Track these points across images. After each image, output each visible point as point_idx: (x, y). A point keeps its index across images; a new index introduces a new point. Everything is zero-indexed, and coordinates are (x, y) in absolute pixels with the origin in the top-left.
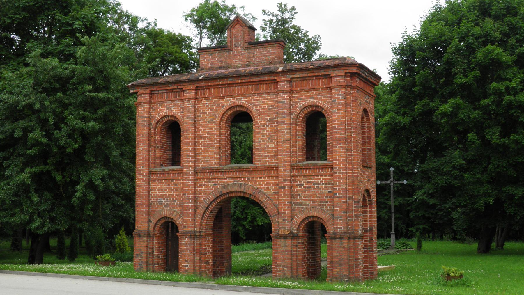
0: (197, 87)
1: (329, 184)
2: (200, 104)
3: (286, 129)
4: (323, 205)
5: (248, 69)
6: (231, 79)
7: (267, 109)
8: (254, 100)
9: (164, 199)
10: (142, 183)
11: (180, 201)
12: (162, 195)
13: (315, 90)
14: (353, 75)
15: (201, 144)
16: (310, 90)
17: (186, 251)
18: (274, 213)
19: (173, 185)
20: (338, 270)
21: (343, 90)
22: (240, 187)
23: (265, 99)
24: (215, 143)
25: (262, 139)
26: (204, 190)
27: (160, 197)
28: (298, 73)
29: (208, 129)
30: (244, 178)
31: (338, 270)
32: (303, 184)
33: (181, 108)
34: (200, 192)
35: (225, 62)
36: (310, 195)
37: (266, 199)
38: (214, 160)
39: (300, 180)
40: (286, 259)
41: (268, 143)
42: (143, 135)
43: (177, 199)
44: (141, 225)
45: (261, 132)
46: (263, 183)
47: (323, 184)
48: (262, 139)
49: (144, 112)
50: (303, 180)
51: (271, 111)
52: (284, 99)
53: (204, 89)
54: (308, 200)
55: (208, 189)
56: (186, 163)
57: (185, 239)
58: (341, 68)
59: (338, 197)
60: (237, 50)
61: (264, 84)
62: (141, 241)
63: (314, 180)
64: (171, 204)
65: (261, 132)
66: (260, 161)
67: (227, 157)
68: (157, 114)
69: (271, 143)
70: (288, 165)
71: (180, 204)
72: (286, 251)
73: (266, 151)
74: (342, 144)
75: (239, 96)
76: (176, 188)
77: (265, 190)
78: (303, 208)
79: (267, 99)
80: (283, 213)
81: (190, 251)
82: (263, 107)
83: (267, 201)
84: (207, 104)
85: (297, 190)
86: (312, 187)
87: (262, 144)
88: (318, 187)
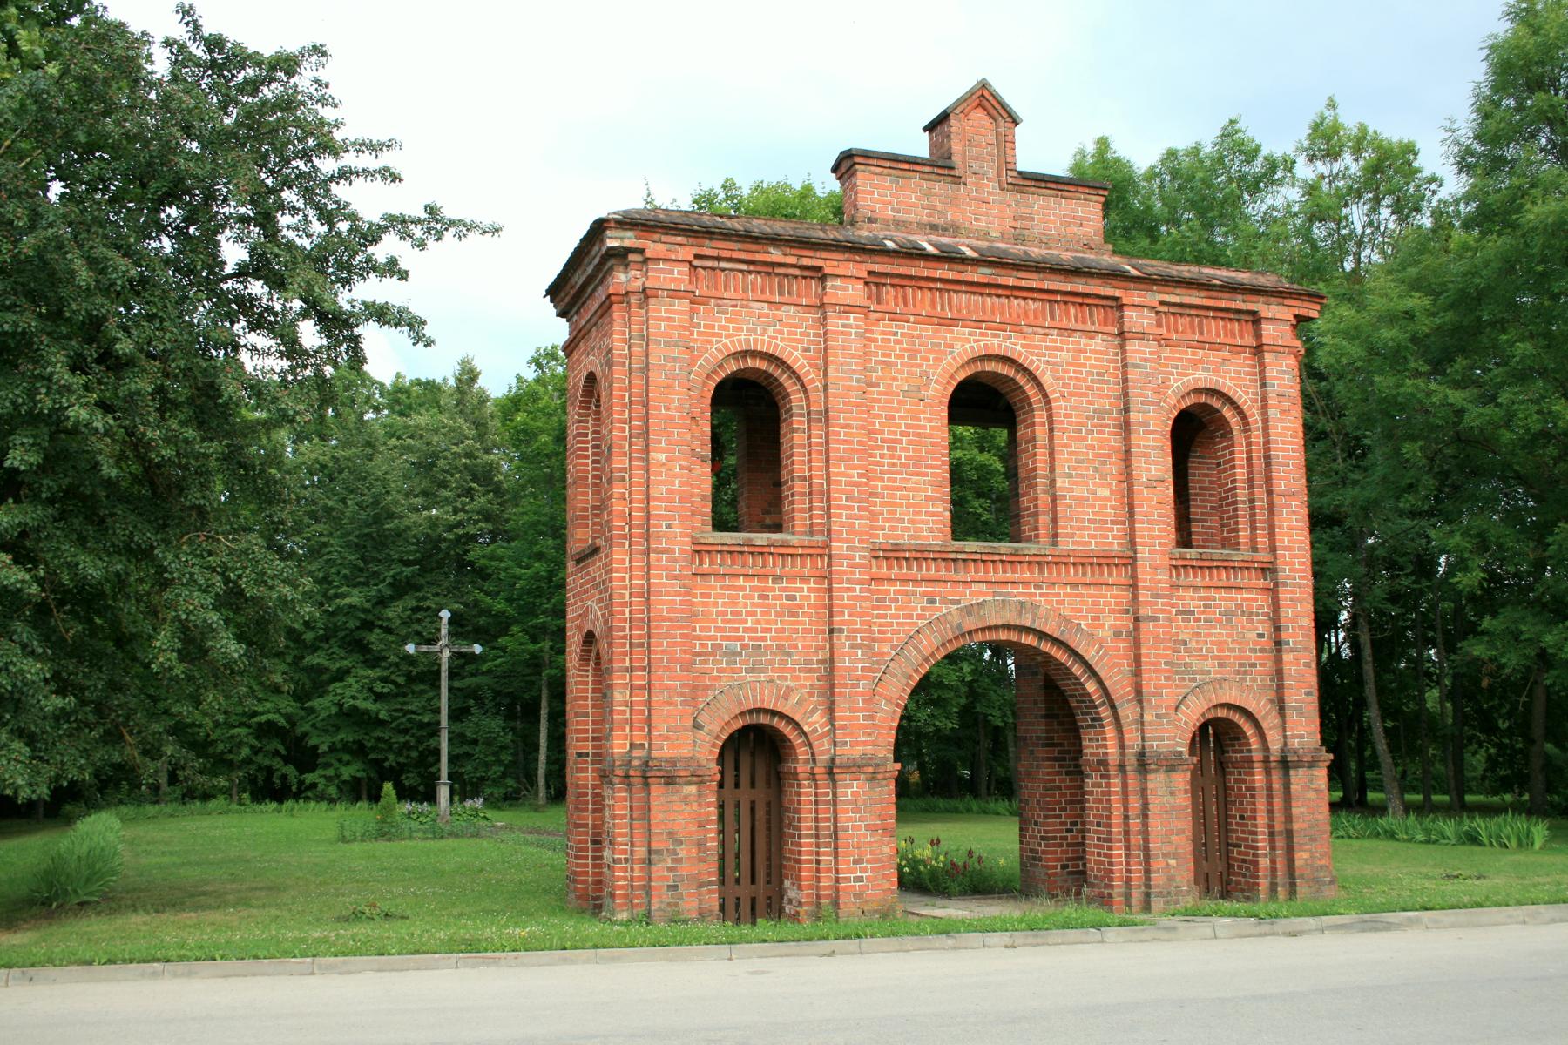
1: (1257, 615)
2: (872, 332)
3: (1153, 448)
4: (1245, 672)
5: (1018, 249)
7: (1085, 380)
8: (1047, 348)
9: (744, 646)
10: (663, 585)
12: (737, 630)
13: (1215, 347)
15: (878, 463)
17: (854, 827)
18: (1123, 696)
19: (779, 598)
20: (1305, 855)
22: (1020, 614)
23: (1081, 351)
25: (1075, 469)
26: (892, 616)
27: (728, 638)
28: (1178, 291)
29: (901, 418)
30: (1025, 583)
31: (1305, 855)
32: (1192, 613)
33: (802, 334)
35: (943, 215)
36: (1213, 643)
38: (927, 522)
39: (1183, 598)
40: (1172, 832)
41: (1094, 484)
42: (668, 409)
43: (795, 647)
44: (667, 738)
45: (1070, 446)
47: (1243, 613)
48: (1075, 469)
49: (673, 327)
50: (1192, 599)
51: (1098, 389)
52: (1145, 360)
54: (1205, 658)
55: (910, 617)
58: (1287, 302)
60: (979, 188)
61: (812, 278)
63: (1222, 600)
64: (771, 662)
65: (1070, 446)
68: (710, 342)
69: (1102, 485)
70: (1163, 553)
71: (807, 662)
72: (1173, 808)
76: (789, 606)
77: (1087, 625)
78: (1194, 680)
79: (1085, 351)
80: (1155, 694)
81: (868, 827)
82: (1075, 372)
83: (1101, 658)
84: (895, 334)
85: (1178, 627)
86: (1217, 620)
87: (1077, 483)
88: (1231, 621)
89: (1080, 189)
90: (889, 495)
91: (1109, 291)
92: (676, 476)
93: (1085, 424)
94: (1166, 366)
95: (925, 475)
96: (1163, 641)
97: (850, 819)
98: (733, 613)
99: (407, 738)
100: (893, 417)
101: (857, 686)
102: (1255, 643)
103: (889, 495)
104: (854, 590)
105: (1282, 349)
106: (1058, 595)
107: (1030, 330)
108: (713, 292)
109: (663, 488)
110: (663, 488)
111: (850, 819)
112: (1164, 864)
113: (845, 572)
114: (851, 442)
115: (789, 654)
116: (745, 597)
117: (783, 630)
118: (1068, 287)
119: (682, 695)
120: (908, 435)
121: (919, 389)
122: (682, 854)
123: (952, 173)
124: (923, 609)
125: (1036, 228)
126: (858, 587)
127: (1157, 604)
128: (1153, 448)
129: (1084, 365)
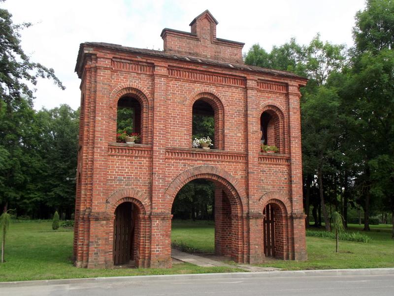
2: (169, 84)
5: (216, 61)
6: (206, 67)
9: (124, 178)
10: (99, 158)
11: (144, 181)
13: (274, 93)
19: (137, 163)
23: (234, 92)
24: (185, 125)
26: (172, 170)
27: (119, 175)
30: (214, 161)
32: (265, 171)
34: (168, 172)
38: (184, 142)
42: (102, 103)
43: (141, 178)
56: (157, 141)
57: (156, 222)
58: (297, 81)
60: (205, 42)
62: (99, 225)
66: (229, 147)
69: (239, 133)
73: (235, 139)
92: (104, 124)
100: (175, 110)
106: (224, 165)
107: (218, 85)
108: (119, 69)
109: (100, 128)
115: (139, 180)
118: (230, 73)
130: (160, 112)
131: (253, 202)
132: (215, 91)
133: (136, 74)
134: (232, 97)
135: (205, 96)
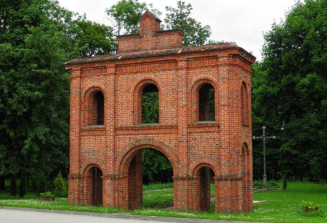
0: (116, 65)
1: (216, 139)
2: (118, 78)
3: (184, 97)
4: (212, 155)
5: (155, 52)
6: (142, 59)
7: (169, 82)
8: (159, 75)
9: (91, 150)
11: (103, 152)
12: (90, 147)
14: (234, 56)
16: (202, 67)
17: (108, 190)
19: (98, 140)
20: (223, 204)
21: (227, 67)
25: (166, 104)
26: (121, 143)
27: (88, 149)
28: (193, 55)
29: (124, 97)
30: (152, 134)
32: (197, 139)
33: (104, 81)
37: (169, 150)
38: (129, 121)
40: (184, 196)
41: (171, 108)
42: (75, 102)
43: (101, 150)
44: (74, 169)
46: (167, 138)
47: (212, 139)
48: (166, 104)
49: (77, 84)
50: (197, 135)
52: (183, 74)
53: (122, 67)
54: (200, 151)
55: (125, 143)
56: (108, 123)
57: (108, 181)
58: (226, 51)
59: (223, 148)
60: (147, 37)
64: (96, 154)
67: (139, 118)
68: (86, 86)
69: (173, 108)
70: (185, 124)
72: (184, 189)
74: (227, 109)
75: (148, 71)
77: (168, 143)
79: (169, 74)
80: (182, 160)
81: (111, 190)
82: (167, 80)
84: (124, 78)
87: (166, 108)
88: (208, 141)
89: (171, 32)
90: (121, 115)
91: (172, 58)
92: (77, 116)
93: (169, 93)
94: (192, 74)
95: (129, 110)
96: (184, 147)
97: (107, 188)
98: (89, 143)
99: (302, 160)
100: (123, 97)
101: (111, 159)
102: (215, 147)
103: (121, 115)
104: (111, 138)
105: (224, 65)
106: (160, 136)
107: (155, 71)
108: (86, 75)
109: (74, 118)
110: (74, 118)
111: (107, 188)
112: (181, 204)
113: (109, 134)
114: (111, 105)
115: (100, 152)
116: (92, 140)
117: (99, 147)
118: (163, 59)
119: (77, 161)
120: (125, 101)
121: (128, 90)
122: (75, 193)
123: (139, 36)
124: (128, 141)
125: (160, 45)
126: (111, 137)
127: (183, 137)
128: (184, 97)
129: (169, 78)
130: (110, 101)
131: (182, 166)
132: (152, 76)
133: (96, 76)
134: (167, 78)
135: (147, 82)
